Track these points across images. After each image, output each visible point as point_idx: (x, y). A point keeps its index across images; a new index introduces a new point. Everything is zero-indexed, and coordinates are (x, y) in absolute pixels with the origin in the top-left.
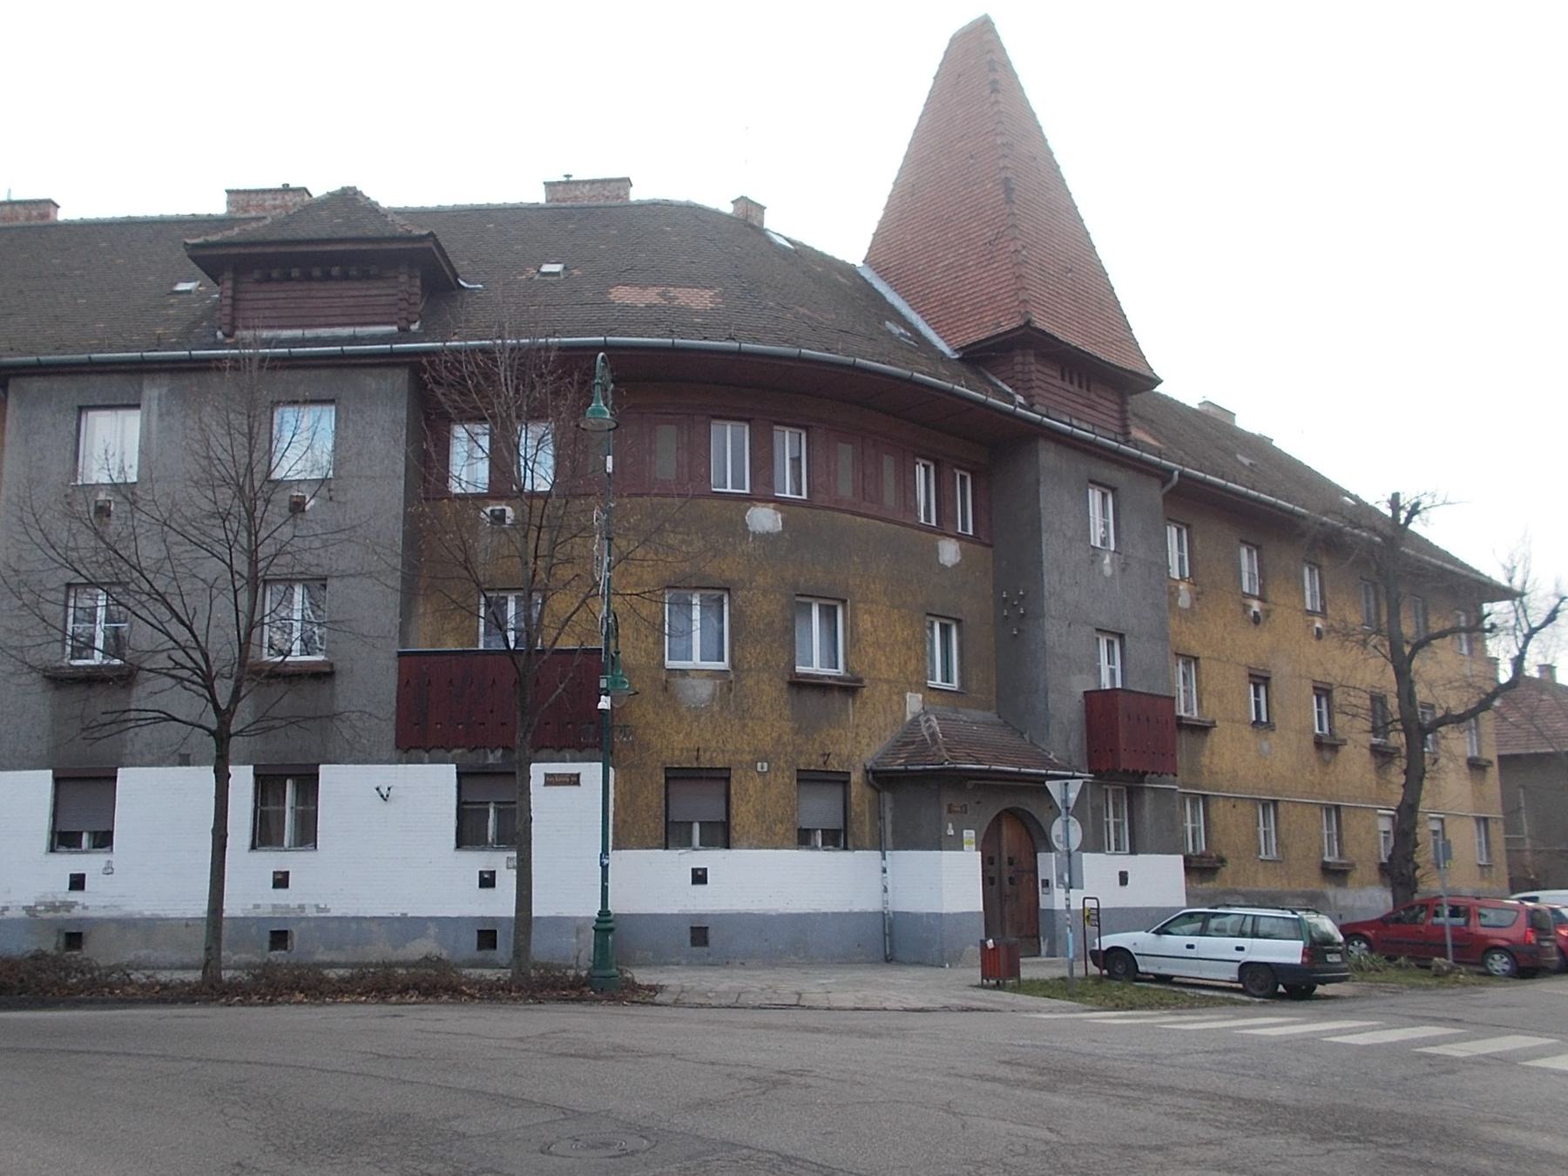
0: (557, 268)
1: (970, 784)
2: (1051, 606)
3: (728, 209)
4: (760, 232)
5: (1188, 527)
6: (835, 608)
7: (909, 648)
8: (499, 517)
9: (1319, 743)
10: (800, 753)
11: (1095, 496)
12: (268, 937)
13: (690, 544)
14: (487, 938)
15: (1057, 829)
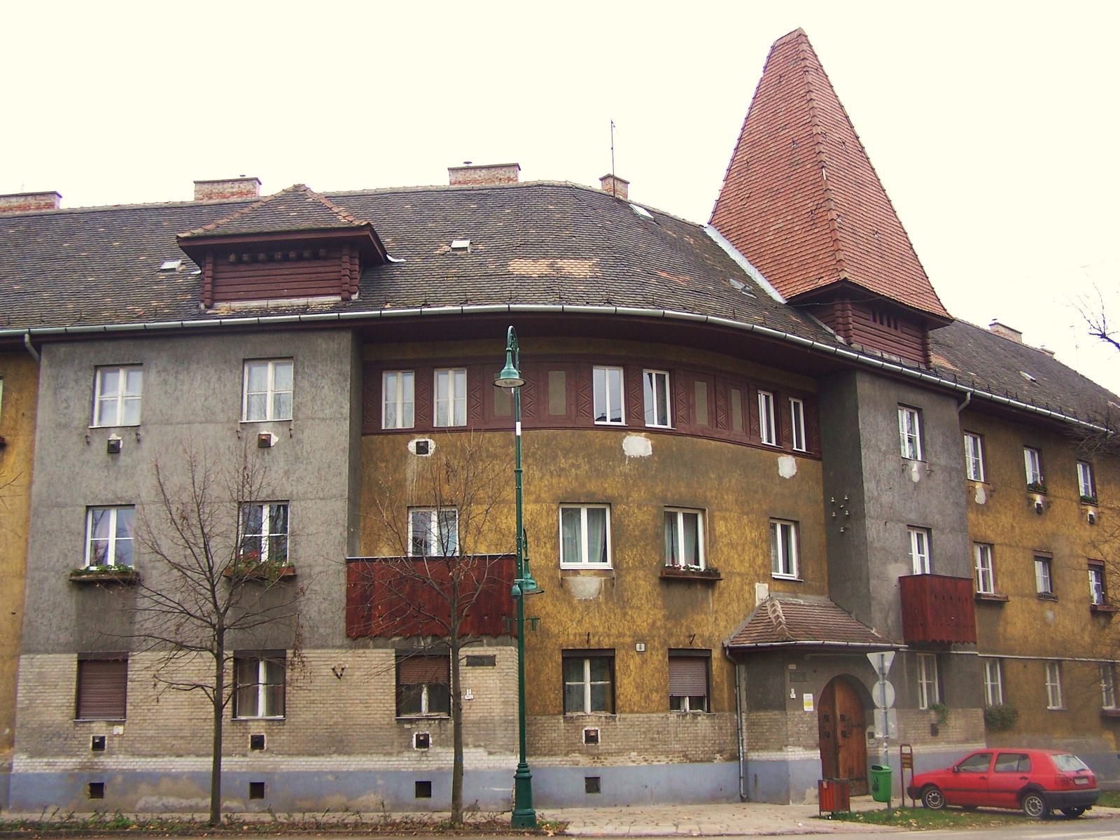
0: (465, 244)
1: (808, 656)
2: (870, 508)
3: (598, 186)
4: (624, 205)
5: (982, 436)
6: (696, 516)
7: (757, 547)
8: (422, 448)
9: (1094, 611)
10: (671, 635)
11: (903, 415)
12: (248, 788)
13: (579, 467)
14: (424, 788)
15: (876, 693)
